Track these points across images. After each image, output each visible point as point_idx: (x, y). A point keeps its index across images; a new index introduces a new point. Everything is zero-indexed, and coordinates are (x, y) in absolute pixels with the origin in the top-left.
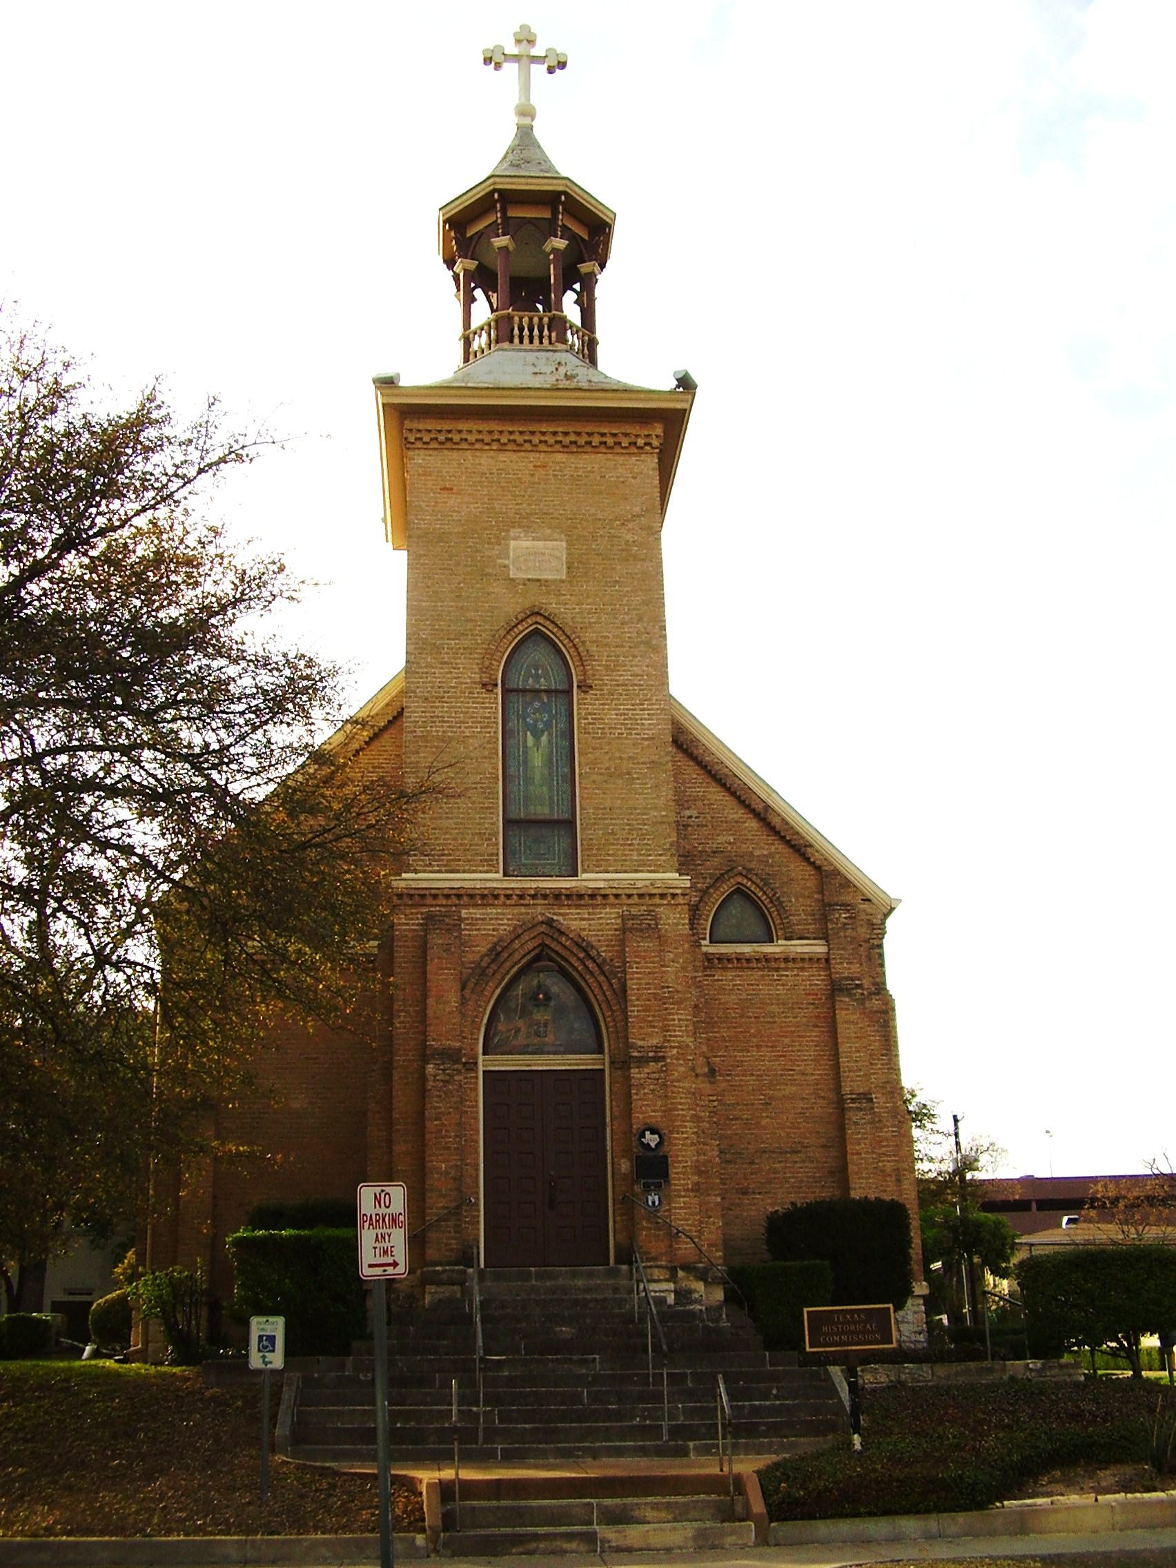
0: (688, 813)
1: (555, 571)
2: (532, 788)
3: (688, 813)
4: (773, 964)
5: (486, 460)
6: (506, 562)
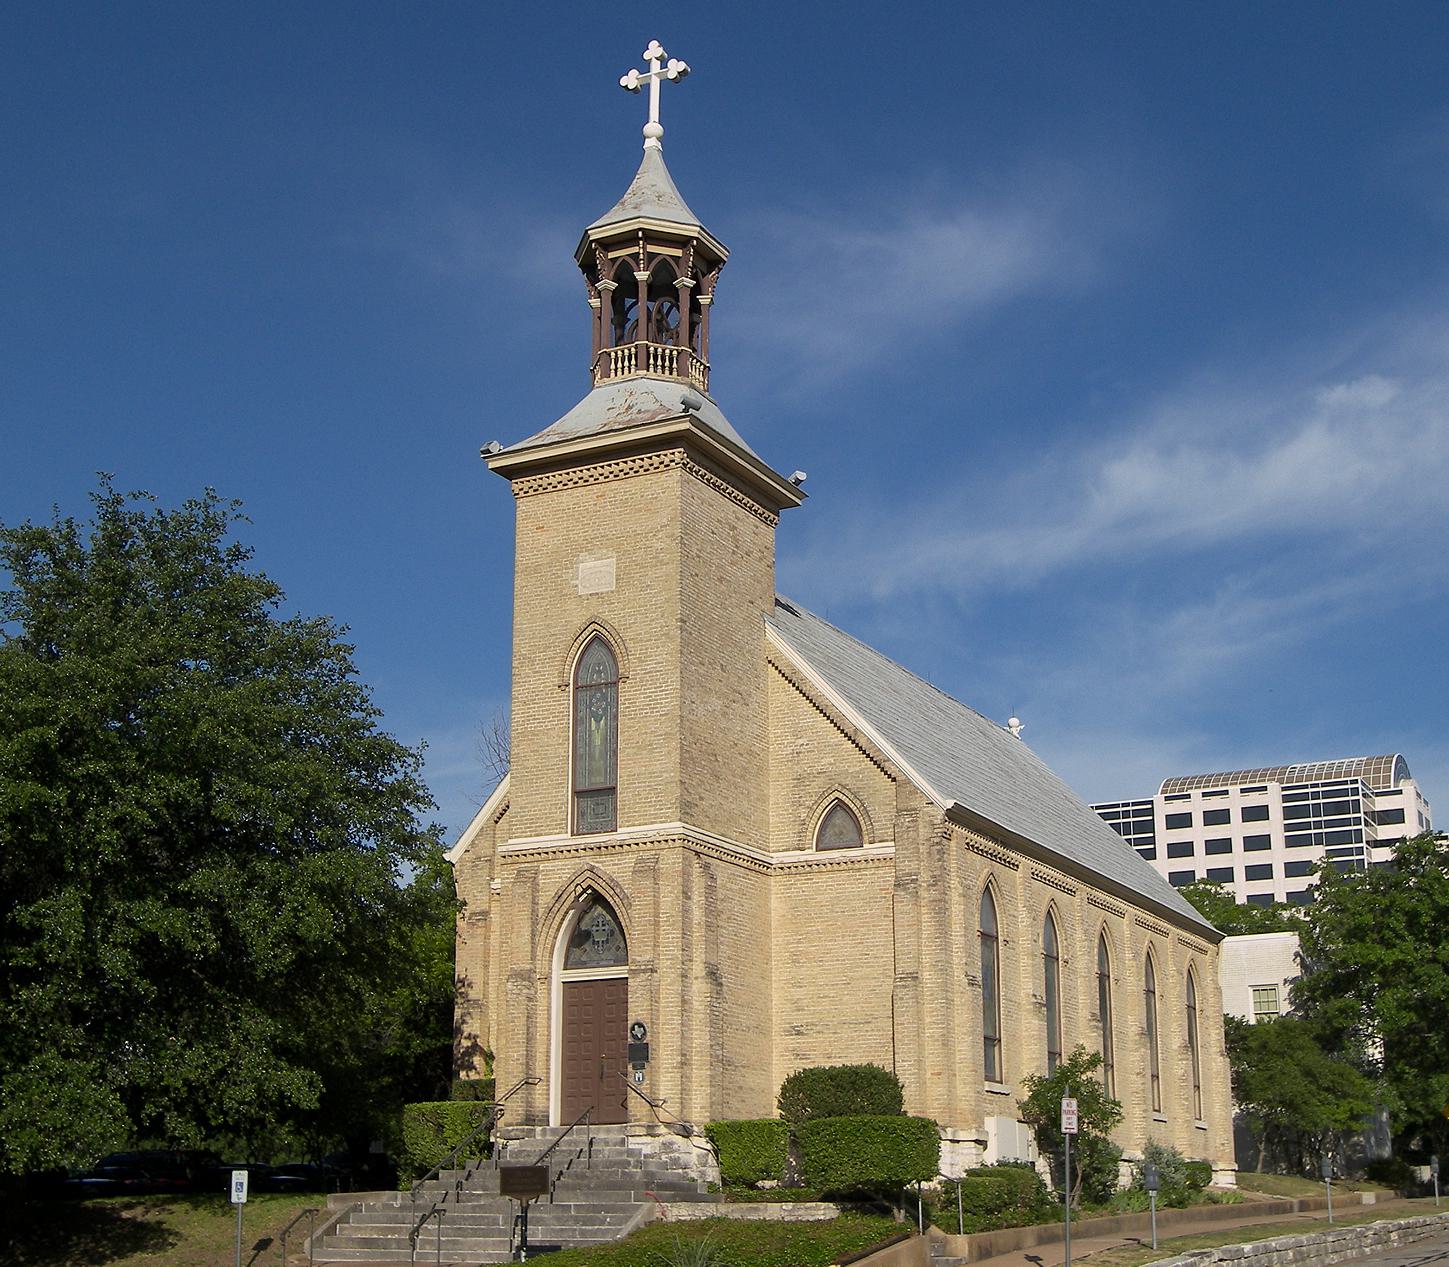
0: (801, 741)
1: (607, 584)
2: (594, 763)
3: (801, 741)
4: (857, 866)
5: (565, 498)
6: (577, 582)
